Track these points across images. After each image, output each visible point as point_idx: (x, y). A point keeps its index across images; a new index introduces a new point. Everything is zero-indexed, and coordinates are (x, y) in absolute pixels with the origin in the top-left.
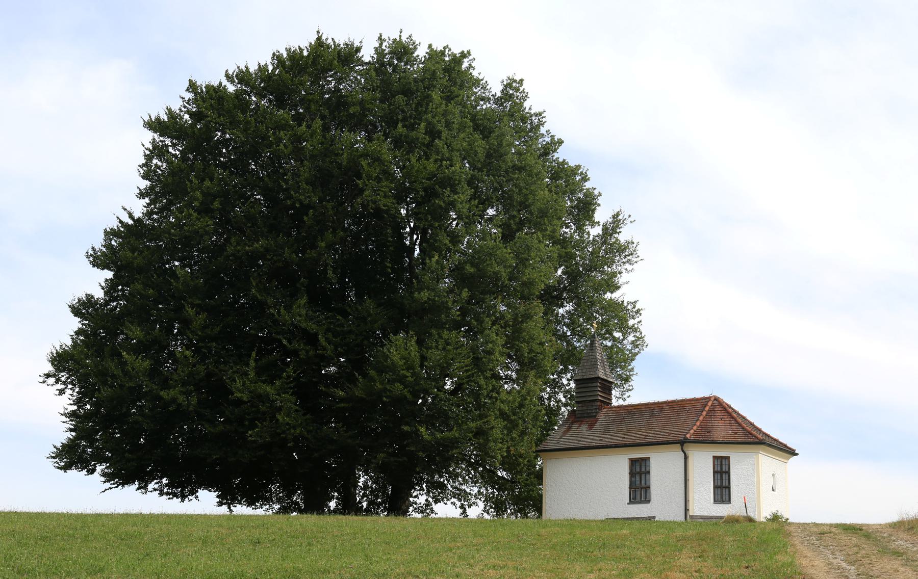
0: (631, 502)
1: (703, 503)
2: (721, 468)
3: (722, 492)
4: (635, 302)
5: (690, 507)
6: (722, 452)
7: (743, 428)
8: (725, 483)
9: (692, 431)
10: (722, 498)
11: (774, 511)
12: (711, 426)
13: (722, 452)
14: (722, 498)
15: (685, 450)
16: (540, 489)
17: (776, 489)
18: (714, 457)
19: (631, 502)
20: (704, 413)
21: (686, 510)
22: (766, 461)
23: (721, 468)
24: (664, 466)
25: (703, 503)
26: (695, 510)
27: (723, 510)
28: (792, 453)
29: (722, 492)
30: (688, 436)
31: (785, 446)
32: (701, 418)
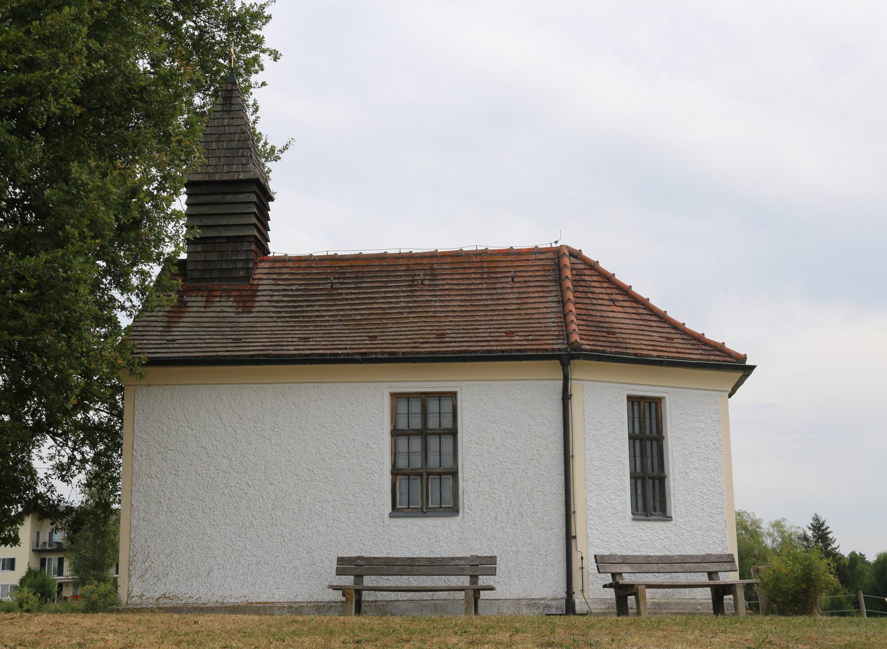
13: (647, 385)
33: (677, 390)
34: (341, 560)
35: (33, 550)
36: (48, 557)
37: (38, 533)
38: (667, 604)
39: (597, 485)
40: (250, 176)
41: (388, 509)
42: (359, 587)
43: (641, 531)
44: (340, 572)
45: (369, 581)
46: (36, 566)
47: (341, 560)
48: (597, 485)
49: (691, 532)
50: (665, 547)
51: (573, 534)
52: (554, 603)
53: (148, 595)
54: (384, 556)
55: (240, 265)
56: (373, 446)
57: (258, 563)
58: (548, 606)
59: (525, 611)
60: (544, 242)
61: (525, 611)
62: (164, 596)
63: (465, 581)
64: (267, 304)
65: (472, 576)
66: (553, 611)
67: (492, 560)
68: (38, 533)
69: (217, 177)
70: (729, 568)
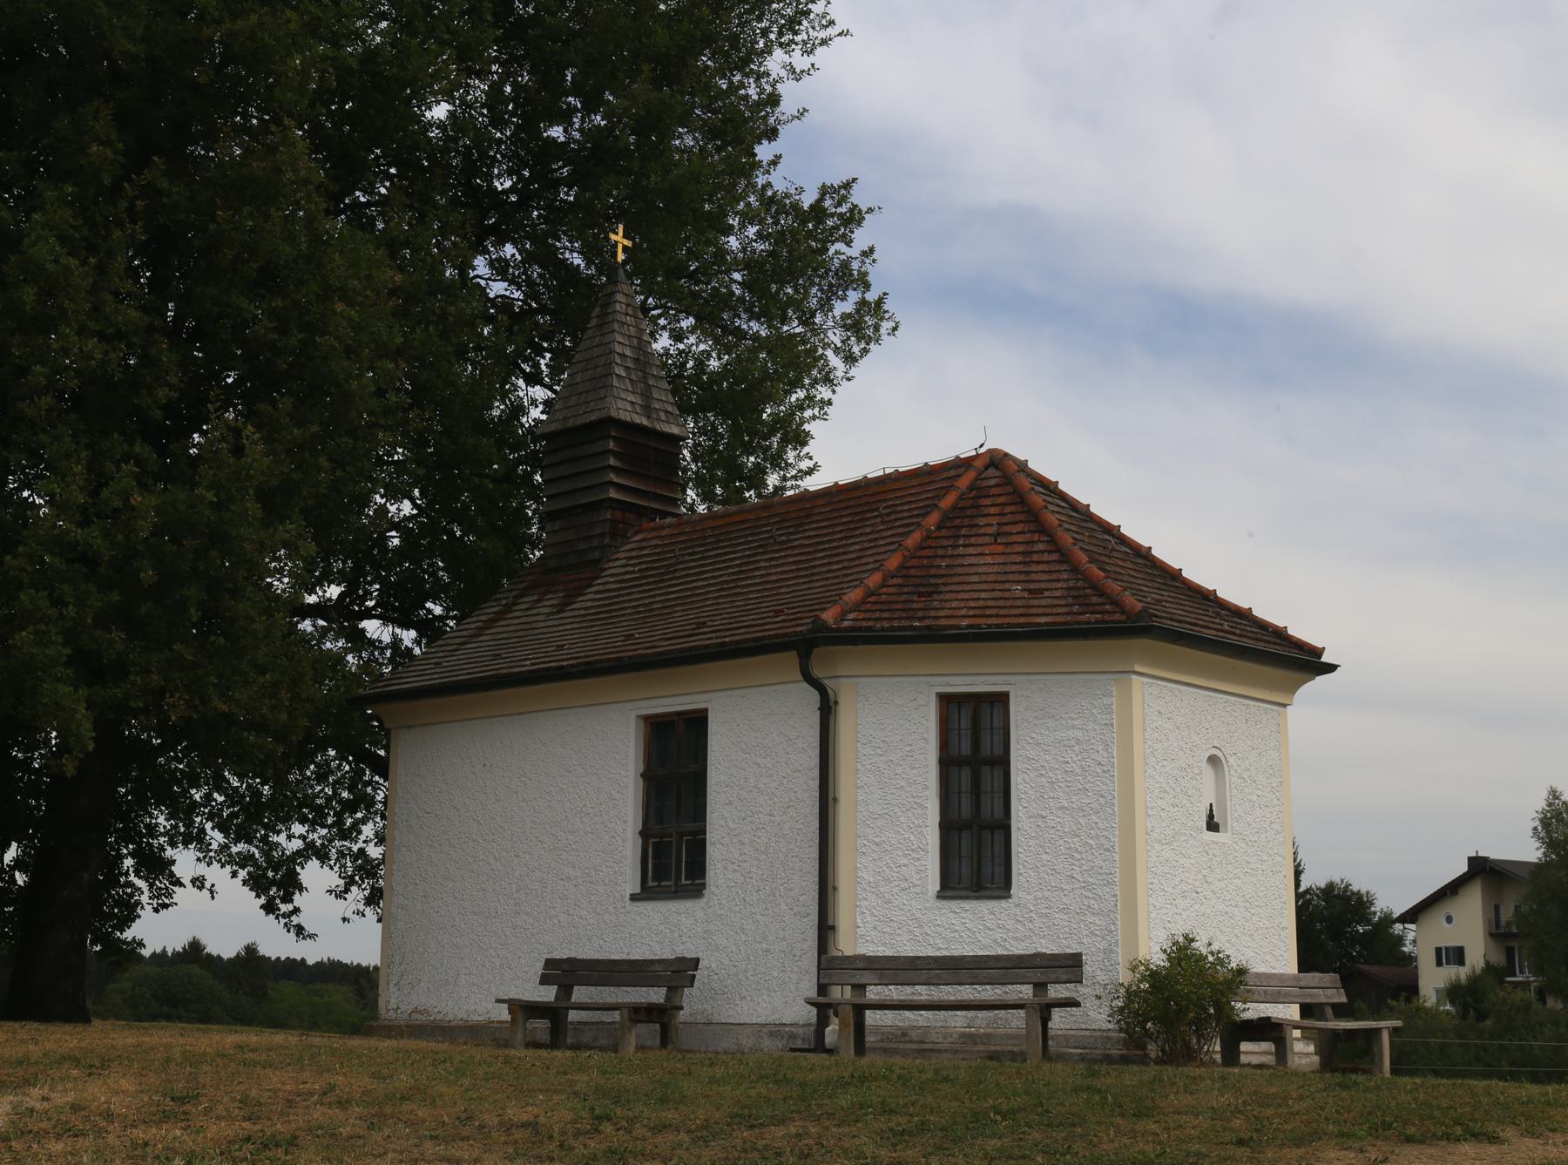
0: (646, 893)
1: (897, 901)
2: (976, 744)
3: (976, 850)
4: (847, 185)
5: (843, 917)
6: (973, 677)
7: (1075, 569)
8: (990, 809)
9: (853, 595)
10: (978, 871)
11: (1179, 929)
12: (1021, 582)
13: (973, 677)
14: (978, 871)
15: (817, 673)
16: (156, 866)
17: (1232, 817)
18: (948, 702)
19: (646, 893)
20: (933, 519)
21: (826, 929)
22: (1167, 717)
23: (976, 744)
24: (755, 743)
25: (897, 901)
26: (862, 934)
27: (975, 928)
28: (1304, 662)
29: (976, 850)
30: (829, 616)
31: (1280, 634)
32: (912, 540)
33: (1030, 677)
34: (550, 963)
35: (1491, 935)
36: (1515, 944)
37: (1497, 908)
38: (988, 1036)
39: (877, 844)
40: (602, 414)
41: (934, 884)
42: (1044, 1000)
43: (952, 916)
44: (545, 980)
45: (580, 994)
46: (1498, 959)
47: (550, 963)
48: (877, 844)
49: (1047, 915)
50: (995, 941)
51: (830, 923)
52: (801, 1031)
53: (403, 1008)
54: (624, 957)
55: (595, 543)
56: (617, 796)
57: (502, 966)
58: (793, 1036)
59: (767, 1043)
60: (965, 449)
61: (767, 1043)
62: (416, 1011)
63: (1026, 992)
64: (1044, 577)
65: (670, 988)
66: (799, 1044)
67: (697, 960)
68: (1497, 908)
69: (570, 424)
70: (1064, 977)
